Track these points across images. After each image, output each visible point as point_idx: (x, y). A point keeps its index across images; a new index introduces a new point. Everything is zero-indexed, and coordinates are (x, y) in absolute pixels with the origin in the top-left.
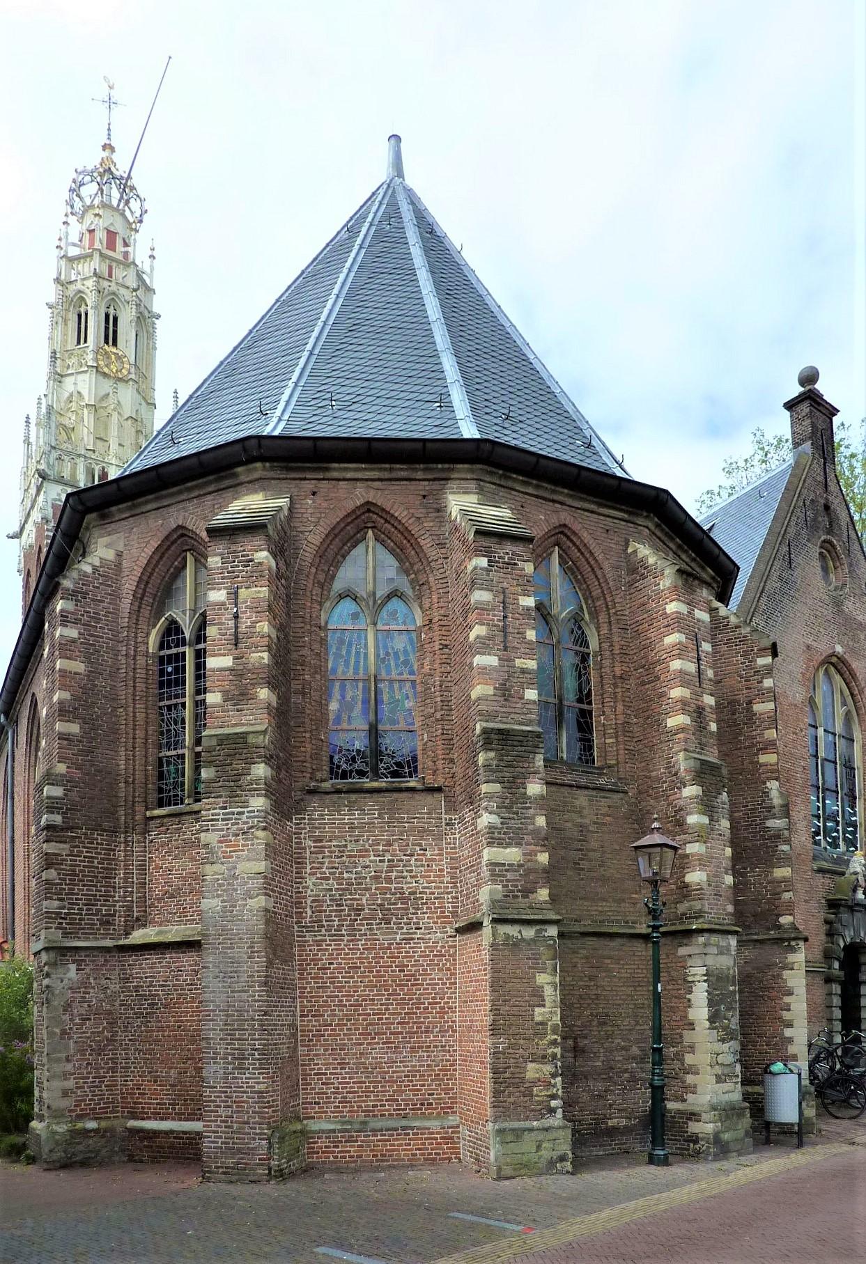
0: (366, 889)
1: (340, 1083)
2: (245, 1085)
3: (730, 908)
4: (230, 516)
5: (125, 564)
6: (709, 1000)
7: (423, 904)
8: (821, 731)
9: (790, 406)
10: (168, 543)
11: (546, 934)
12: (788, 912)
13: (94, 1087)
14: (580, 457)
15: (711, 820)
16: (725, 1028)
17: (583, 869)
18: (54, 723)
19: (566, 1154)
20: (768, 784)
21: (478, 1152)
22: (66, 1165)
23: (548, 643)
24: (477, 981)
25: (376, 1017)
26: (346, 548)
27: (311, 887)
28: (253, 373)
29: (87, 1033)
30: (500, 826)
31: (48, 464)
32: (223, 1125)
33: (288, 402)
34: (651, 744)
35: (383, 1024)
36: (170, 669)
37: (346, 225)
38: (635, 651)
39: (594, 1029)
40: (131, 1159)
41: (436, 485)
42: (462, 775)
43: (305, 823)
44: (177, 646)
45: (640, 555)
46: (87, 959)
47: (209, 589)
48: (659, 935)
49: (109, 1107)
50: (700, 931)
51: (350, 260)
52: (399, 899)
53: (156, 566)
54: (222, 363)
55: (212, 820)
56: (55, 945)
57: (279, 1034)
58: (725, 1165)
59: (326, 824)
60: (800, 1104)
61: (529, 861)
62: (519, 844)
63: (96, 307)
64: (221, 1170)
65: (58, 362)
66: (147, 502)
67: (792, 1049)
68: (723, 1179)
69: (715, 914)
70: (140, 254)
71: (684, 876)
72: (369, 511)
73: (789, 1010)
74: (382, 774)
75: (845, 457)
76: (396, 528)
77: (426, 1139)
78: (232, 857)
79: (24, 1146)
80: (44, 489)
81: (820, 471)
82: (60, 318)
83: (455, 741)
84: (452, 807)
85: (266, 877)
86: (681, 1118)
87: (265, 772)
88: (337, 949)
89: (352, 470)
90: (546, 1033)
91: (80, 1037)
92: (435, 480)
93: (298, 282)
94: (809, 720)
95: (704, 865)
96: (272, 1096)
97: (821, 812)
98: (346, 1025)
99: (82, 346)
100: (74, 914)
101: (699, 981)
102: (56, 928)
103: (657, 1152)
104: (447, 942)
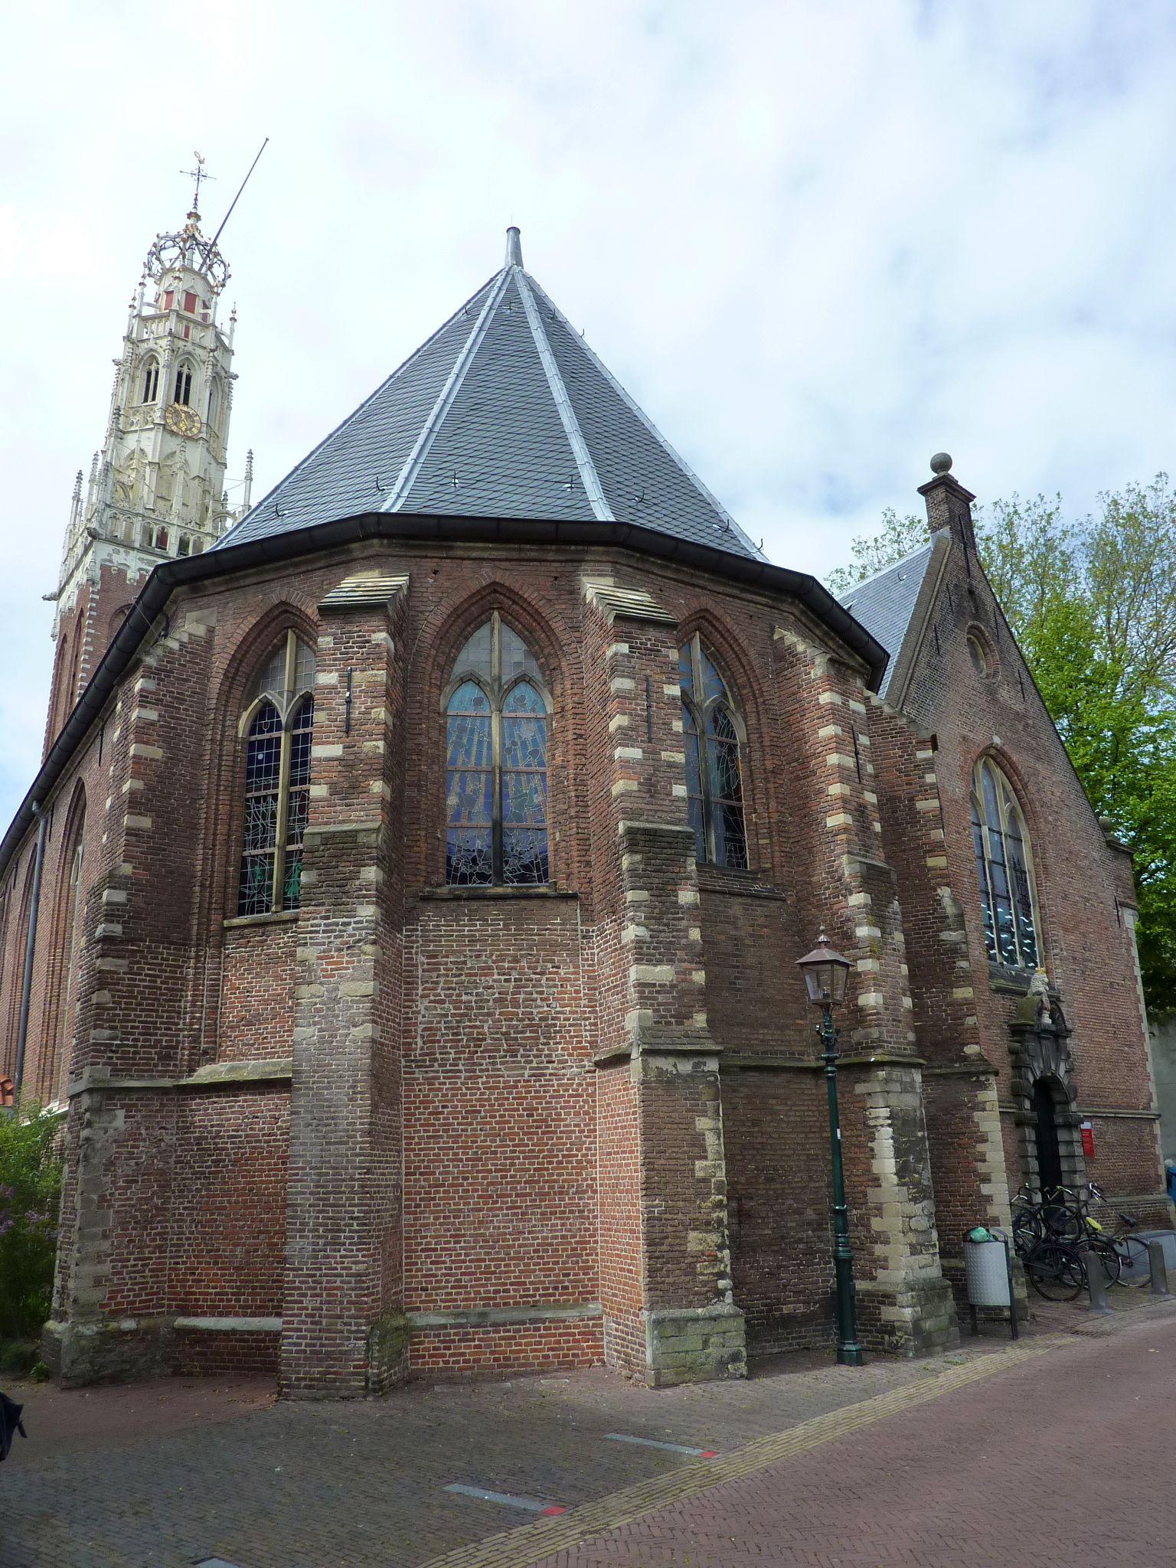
0: (489, 1015)
1: (453, 1262)
2: (339, 1266)
3: (911, 1036)
4: (344, 594)
5: (217, 640)
6: (895, 1148)
7: (556, 1032)
8: (985, 830)
9: (924, 490)
10: (268, 620)
11: (706, 1069)
12: (973, 1041)
13: (135, 1272)
14: (717, 541)
15: (882, 933)
16: (917, 1184)
17: (739, 990)
18: (121, 815)
19: (739, 1353)
20: (939, 891)
21: (629, 1351)
22: (91, 1382)
23: (693, 737)
24: (625, 1127)
25: (499, 1174)
26: (469, 629)
27: (423, 1012)
28: (368, 447)
29: (132, 1199)
30: (649, 939)
31: (101, 523)
32: (309, 1320)
33: (407, 479)
34: (810, 845)
35: (507, 1183)
36: (260, 757)
37: (464, 307)
38: (786, 743)
39: (762, 1186)
40: (177, 1372)
41: (569, 567)
42: (601, 880)
43: (417, 936)
44: (270, 730)
45: (787, 643)
46: (139, 1103)
47: (318, 671)
48: (834, 1069)
49: (152, 1300)
50: (880, 1065)
51: (470, 342)
52: (528, 1026)
53: (252, 644)
54: (331, 436)
55: (311, 932)
56: (101, 1085)
57: (382, 1198)
58: (933, 1363)
59: (442, 936)
60: (1010, 1280)
61: (682, 981)
62: (671, 961)
63: (168, 366)
64: (303, 1384)
65: (122, 418)
66: (247, 576)
67: (992, 1211)
68: (931, 1381)
69: (895, 1043)
70: (220, 316)
71: (857, 999)
72: (495, 591)
73: (984, 1161)
74: (507, 878)
75: (981, 539)
76: (525, 610)
77: (561, 1335)
78: (333, 976)
79: (34, 1357)
80: (93, 549)
81: (961, 555)
82: (127, 376)
83: (592, 841)
84: (589, 918)
85: (373, 1001)
86: (873, 1301)
87: (377, 875)
88: (452, 1089)
89: (478, 549)
90: (709, 1194)
91: (123, 1206)
92: (566, 561)
93: (414, 359)
94: (971, 818)
95: (880, 986)
96: (372, 1280)
97: (993, 922)
98: (462, 1185)
99: (149, 403)
100: (128, 1046)
101: (882, 1126)
102: (105, 1064)
103: (847, 1347)
104: (585, 1079)
